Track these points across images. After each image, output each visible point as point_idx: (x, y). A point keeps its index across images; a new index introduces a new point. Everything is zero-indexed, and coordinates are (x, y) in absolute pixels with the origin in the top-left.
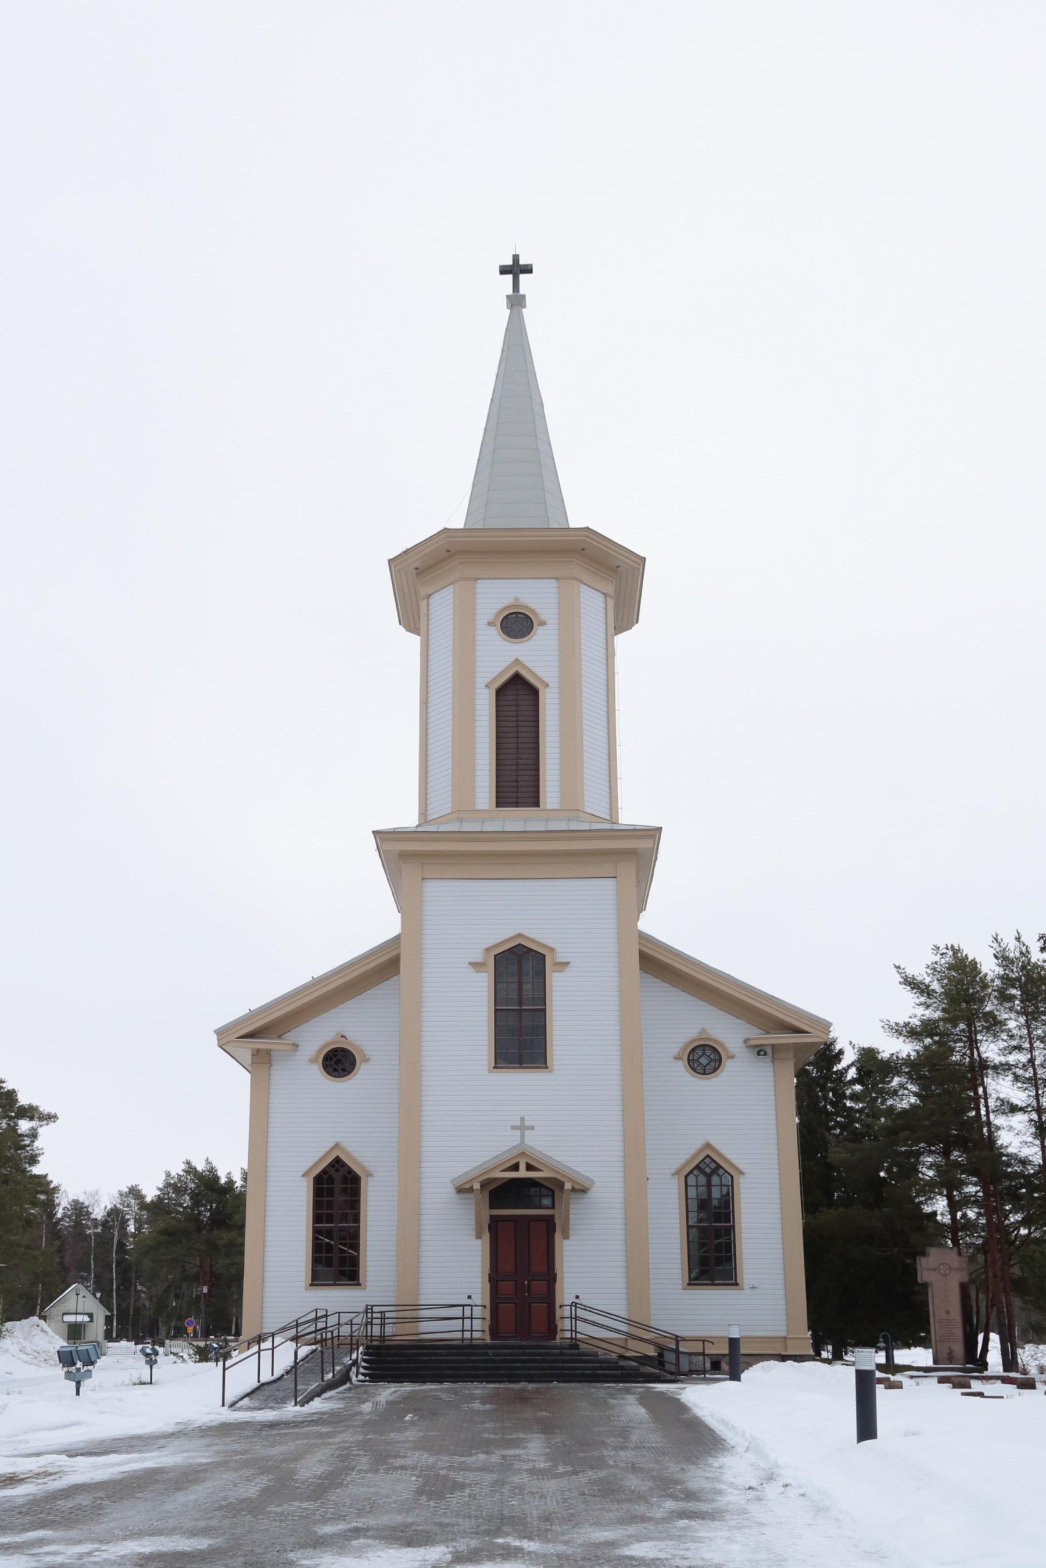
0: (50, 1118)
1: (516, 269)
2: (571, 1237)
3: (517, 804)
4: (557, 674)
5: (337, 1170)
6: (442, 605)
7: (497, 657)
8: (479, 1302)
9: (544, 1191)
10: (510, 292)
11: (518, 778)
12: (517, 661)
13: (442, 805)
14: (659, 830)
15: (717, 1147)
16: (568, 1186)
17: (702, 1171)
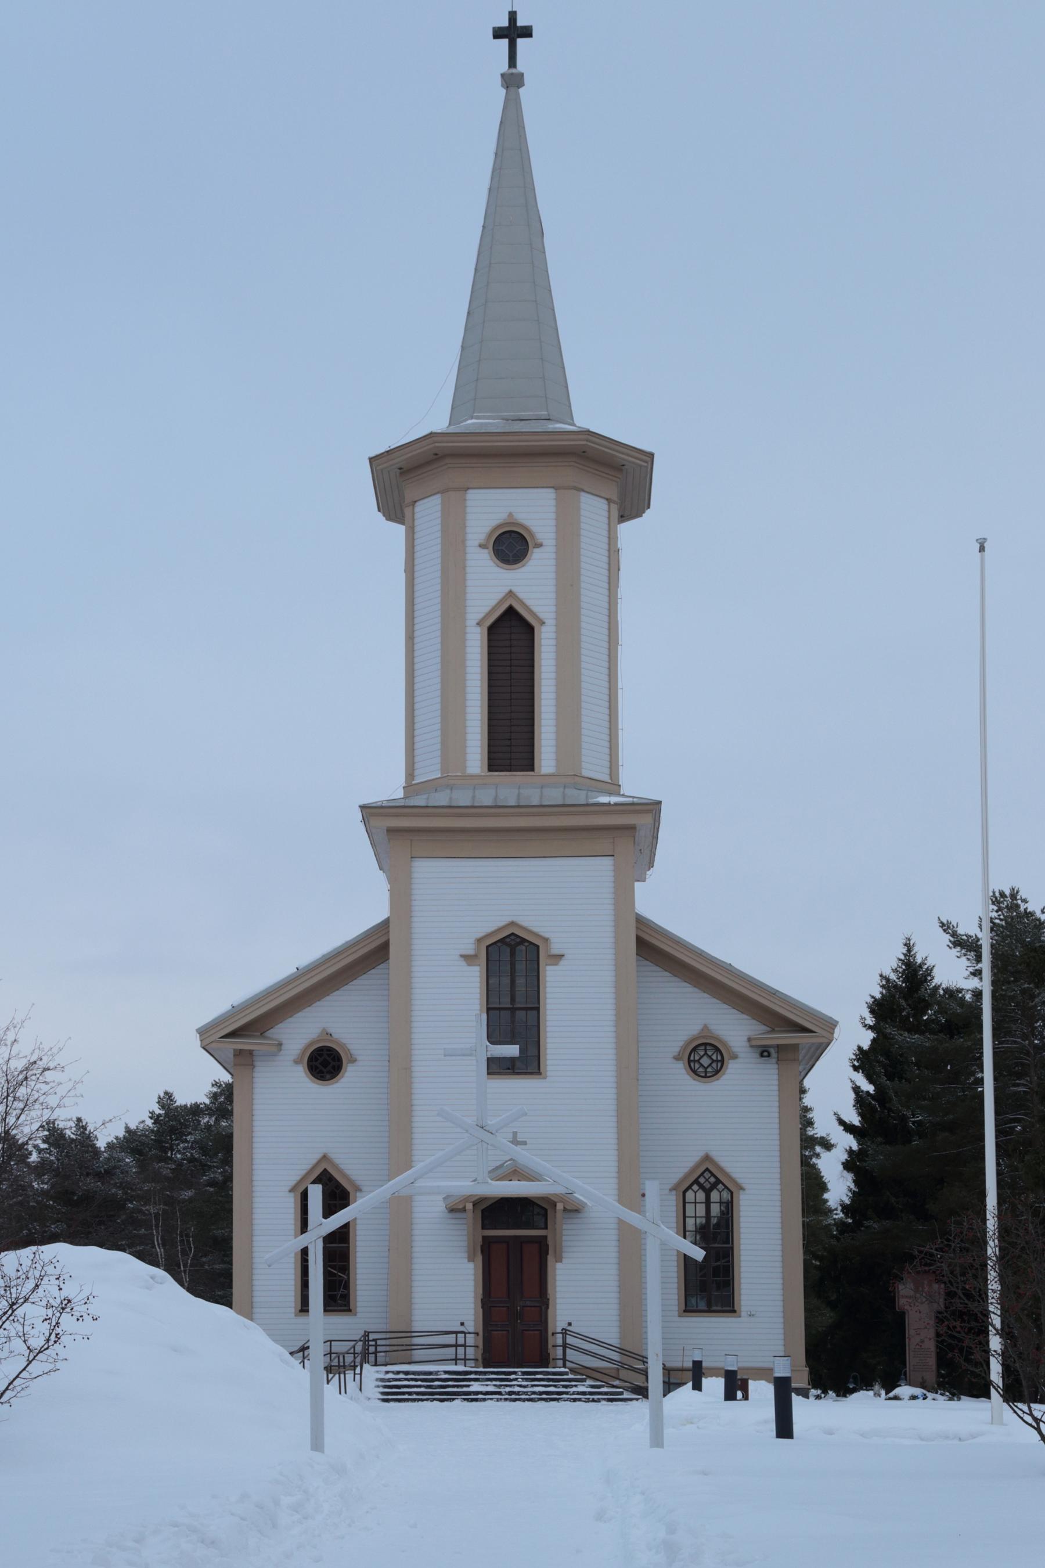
1: (513, 32)
3: (510, 768)
6: (429, 511)
7: (489, 585)
8: (472, 1330)
9: (537, 1210)
10: (504, 67)
11: (511, 741)
12: (511, 594)
14: (660, 802)
16: (560, 1206)
17: (701, 1187)
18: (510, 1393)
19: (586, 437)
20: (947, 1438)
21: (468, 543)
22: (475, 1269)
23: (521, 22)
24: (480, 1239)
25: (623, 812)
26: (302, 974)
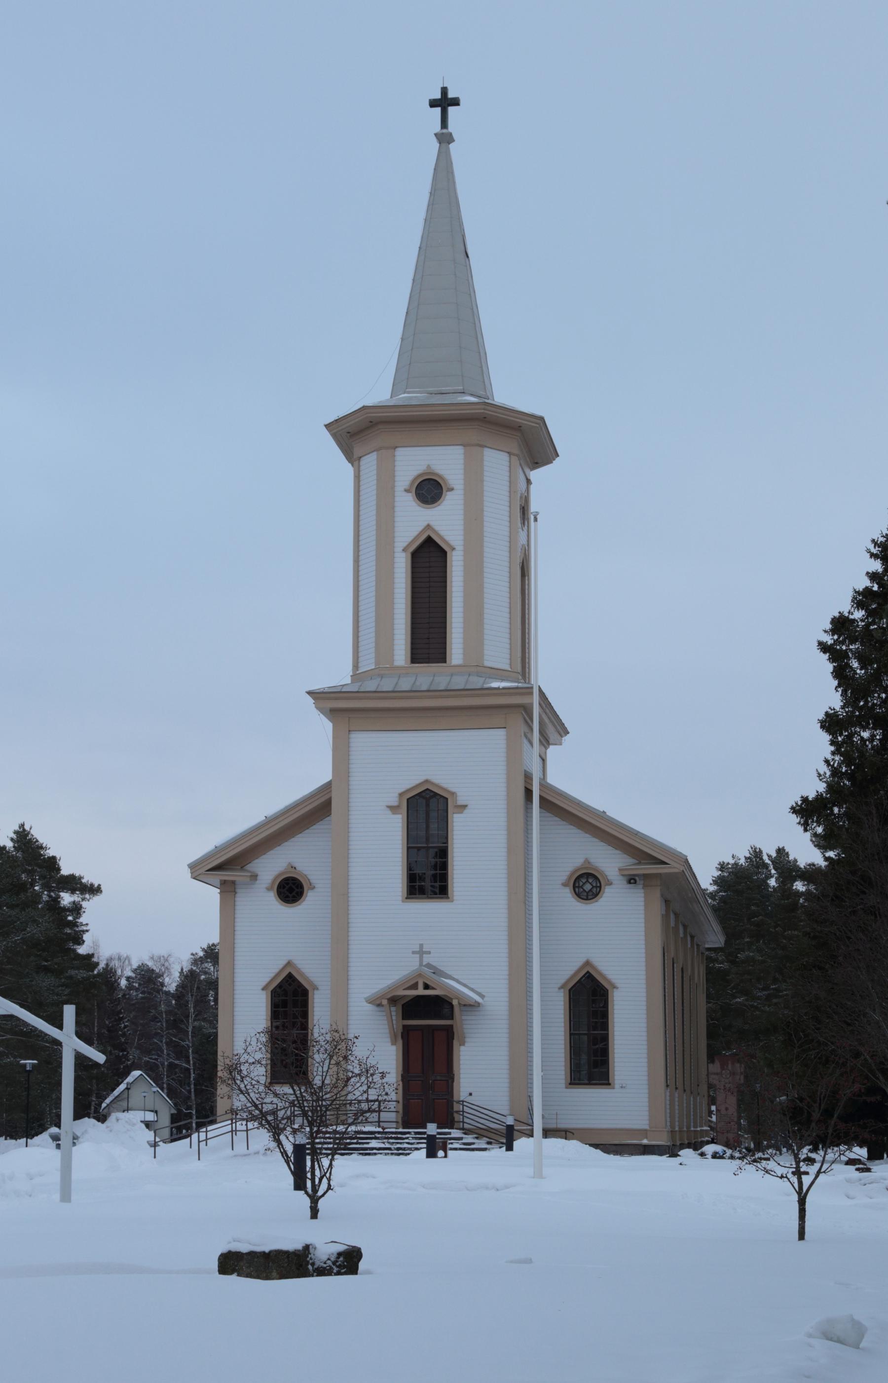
0: (94, 890)
1: (444, 102)
2: (466, 1044)
3: (428, 660)
4: (462, 538)
5: (290, 985)
6: (370, 462)
7: (412, 520)
10: (437, 128)
11: (429, 639)
13: (368, 664)
18: (398, 1149)
19: (483, 407)
20: (487, 1188)
21: (397, 489)
23: (451, 95)
24: (401, 1027)
25: (511, 694)
26: (269, 821)
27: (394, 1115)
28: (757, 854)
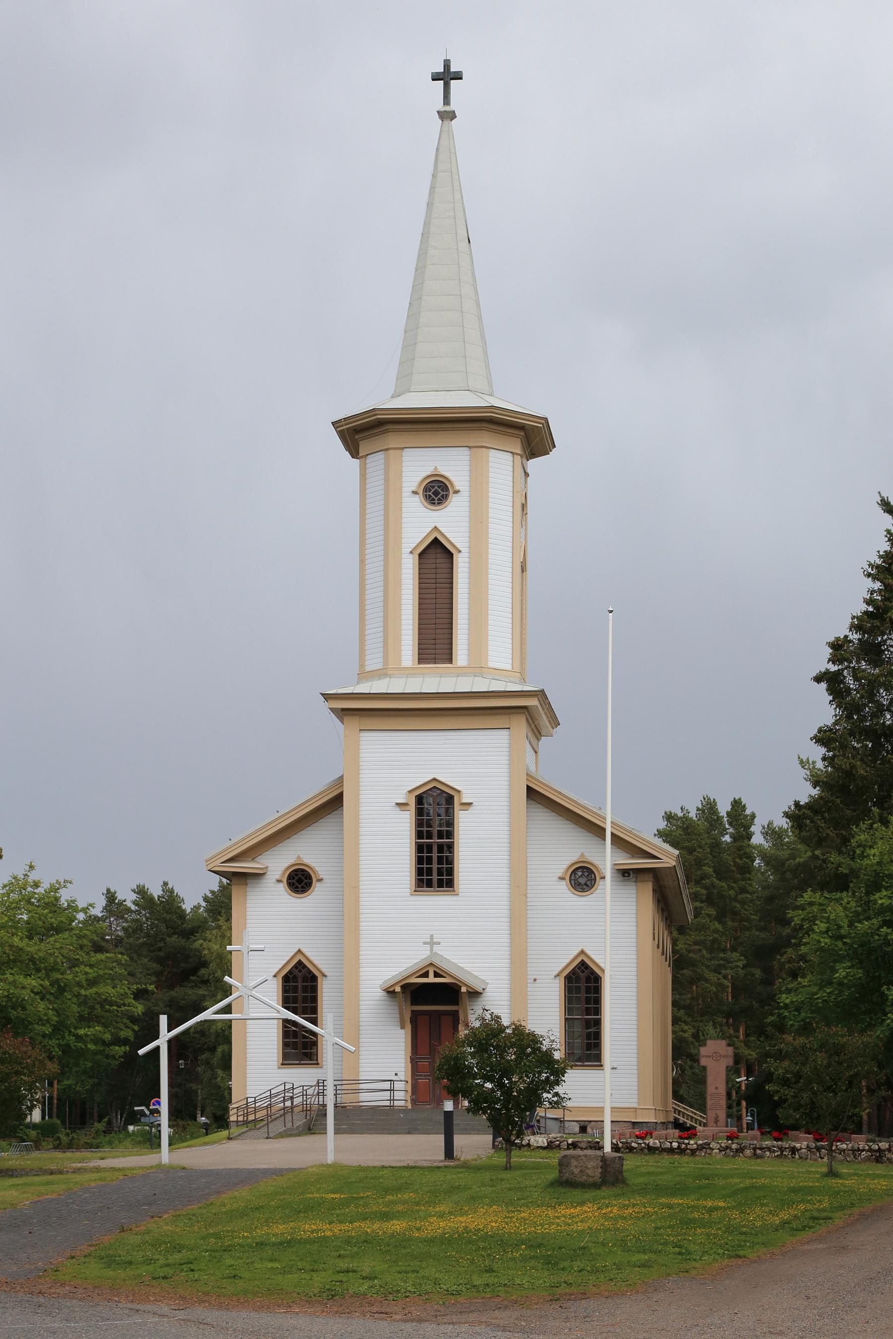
1: (447, 76)
3: (435, 661)
7: (418, 522)
10: (440, 106)
15: (589, 953)
16: (464, 989)
22: (406, 1034)
27: (403, 1093)
28: (709, 808)
